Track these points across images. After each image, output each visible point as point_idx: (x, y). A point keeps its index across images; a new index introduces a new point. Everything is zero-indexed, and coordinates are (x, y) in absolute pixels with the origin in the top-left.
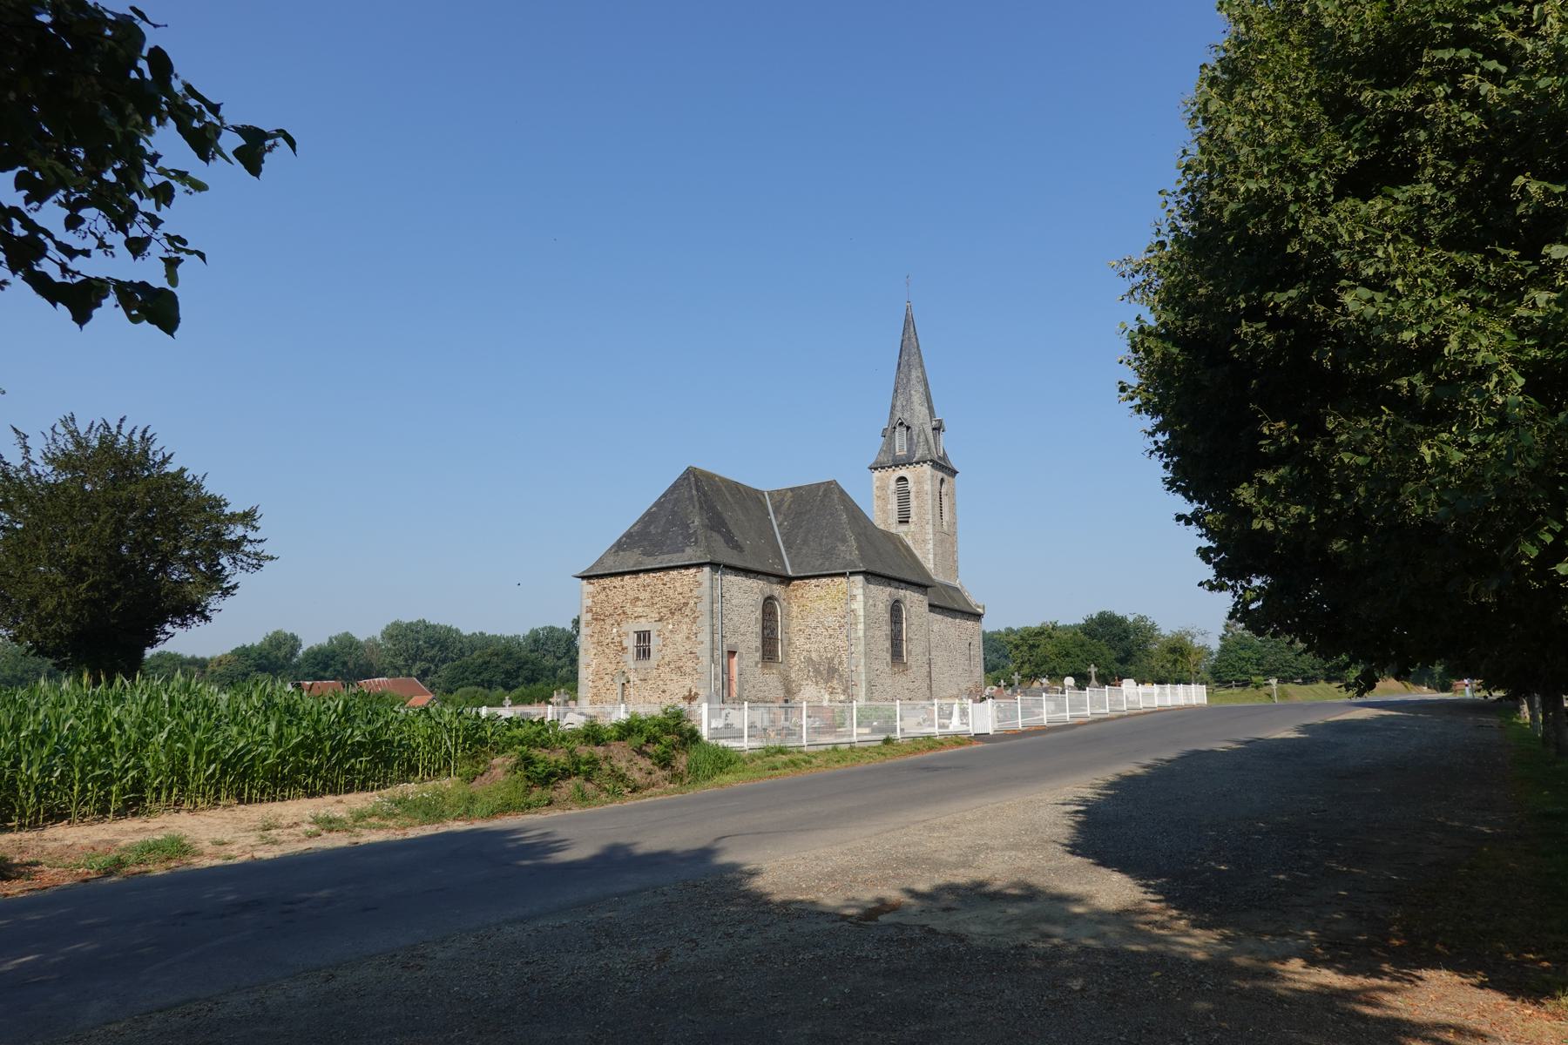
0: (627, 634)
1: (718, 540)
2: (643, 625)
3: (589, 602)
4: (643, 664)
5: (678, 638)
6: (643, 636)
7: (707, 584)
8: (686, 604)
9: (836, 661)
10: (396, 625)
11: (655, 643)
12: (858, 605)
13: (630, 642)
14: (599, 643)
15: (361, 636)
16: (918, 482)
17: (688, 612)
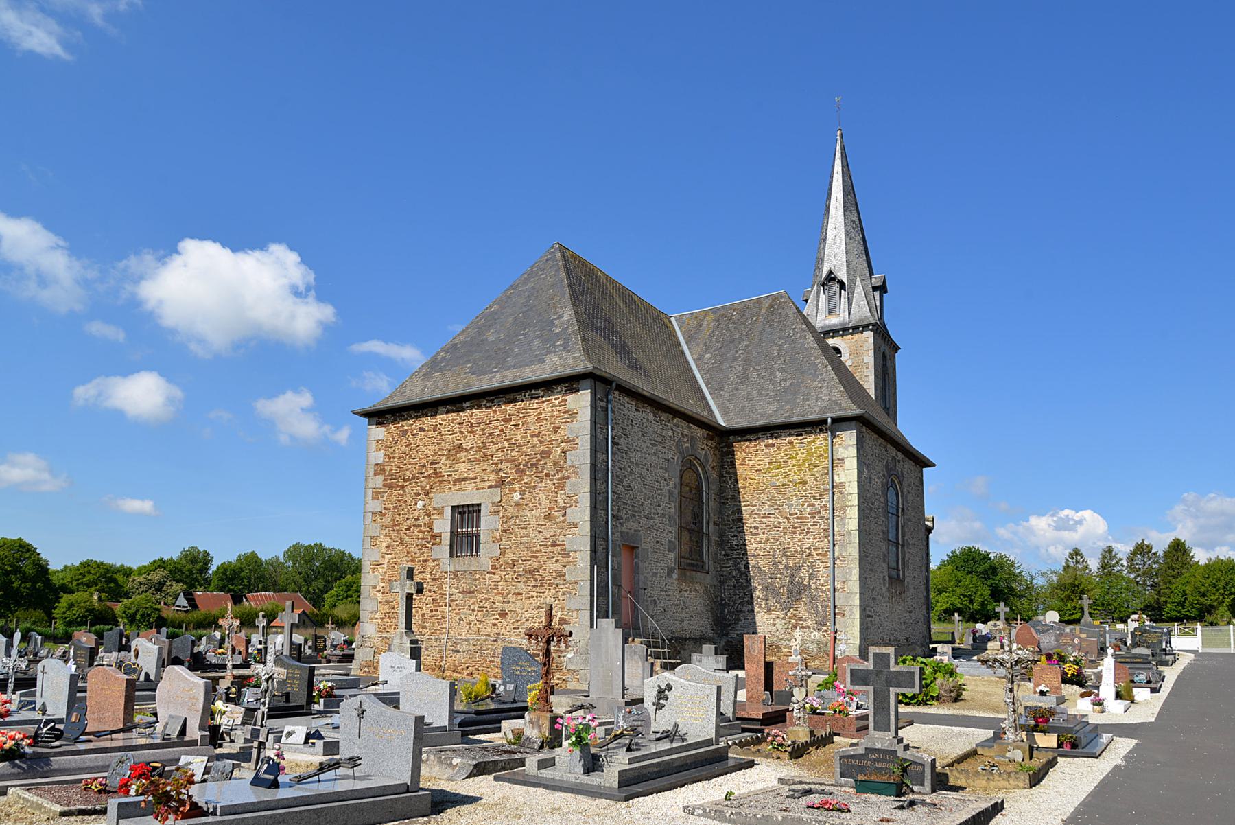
0: (440, 511)
1: (607, 352)
2: (466, 496)
3: (379, 457)
4: (465, 564)
5: (533, 516)
6: (466, 513)
7: (585, 415)
8: (546, 455)
9: (805, 572)
10: (297, 547)
11: (488, 524)
12: (848, 476)
13: (443, 526)
14: (394, 526)
15: (264, 556)
16: (857, 353)
17: (549, 468)
